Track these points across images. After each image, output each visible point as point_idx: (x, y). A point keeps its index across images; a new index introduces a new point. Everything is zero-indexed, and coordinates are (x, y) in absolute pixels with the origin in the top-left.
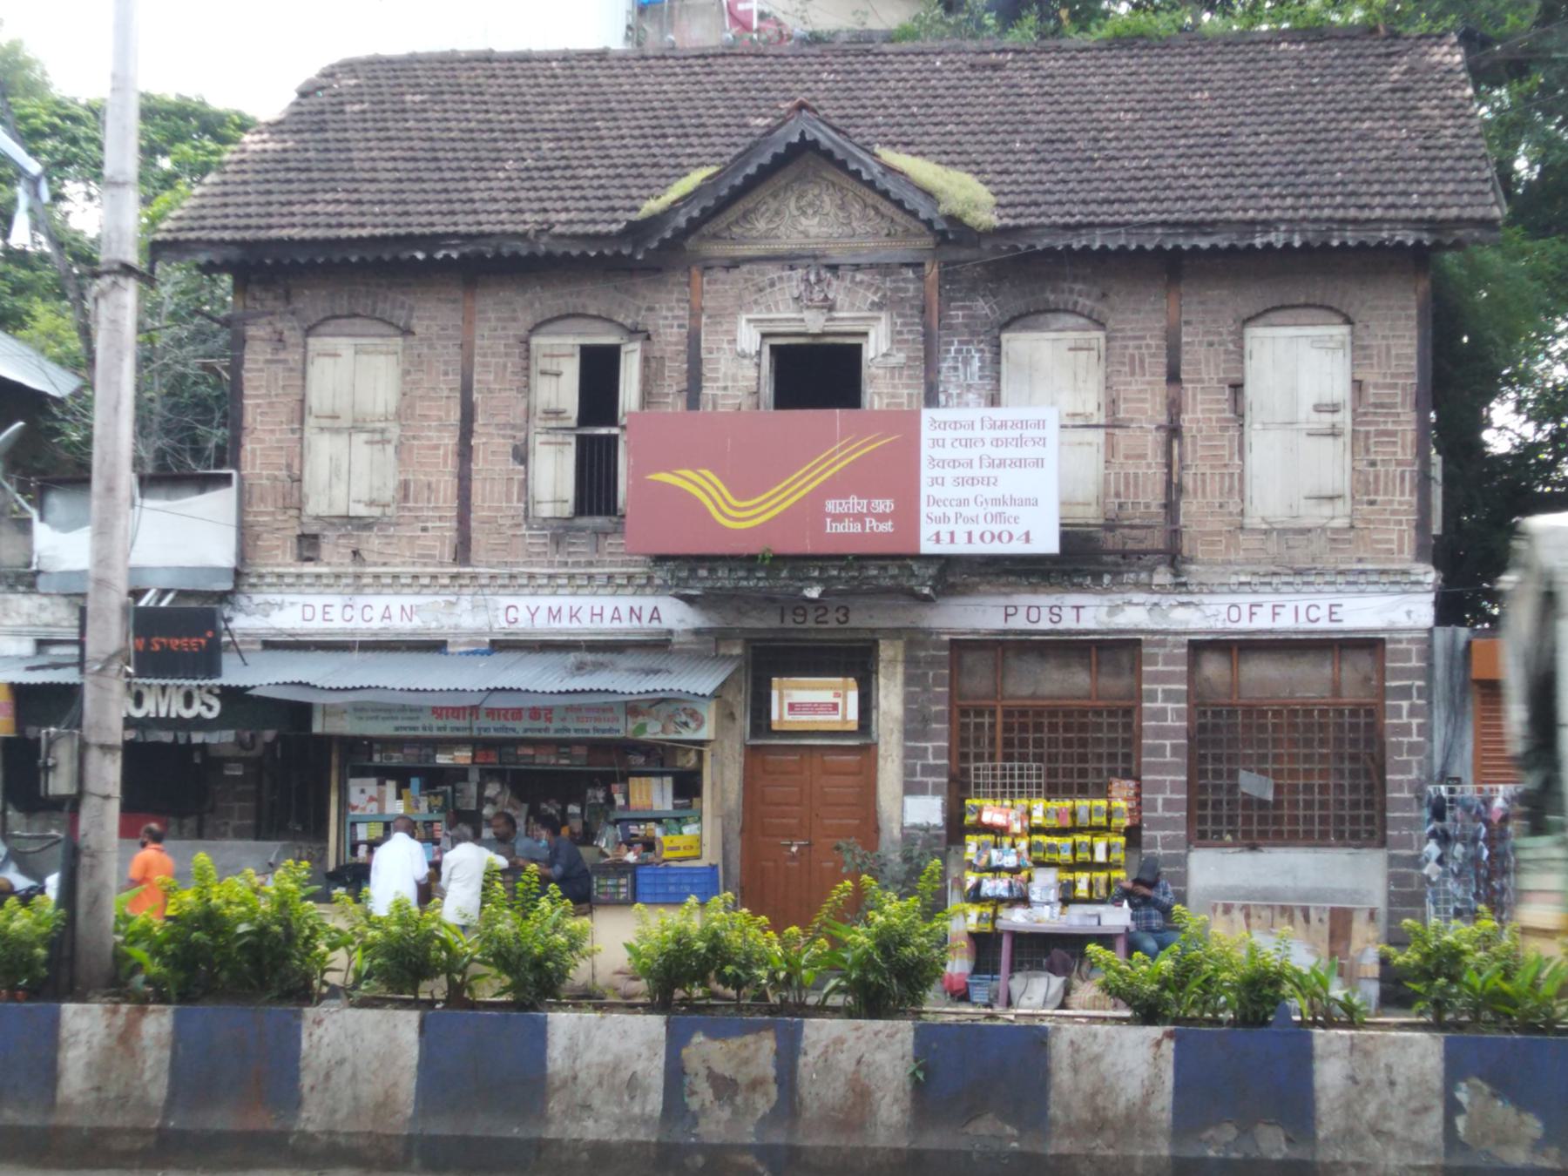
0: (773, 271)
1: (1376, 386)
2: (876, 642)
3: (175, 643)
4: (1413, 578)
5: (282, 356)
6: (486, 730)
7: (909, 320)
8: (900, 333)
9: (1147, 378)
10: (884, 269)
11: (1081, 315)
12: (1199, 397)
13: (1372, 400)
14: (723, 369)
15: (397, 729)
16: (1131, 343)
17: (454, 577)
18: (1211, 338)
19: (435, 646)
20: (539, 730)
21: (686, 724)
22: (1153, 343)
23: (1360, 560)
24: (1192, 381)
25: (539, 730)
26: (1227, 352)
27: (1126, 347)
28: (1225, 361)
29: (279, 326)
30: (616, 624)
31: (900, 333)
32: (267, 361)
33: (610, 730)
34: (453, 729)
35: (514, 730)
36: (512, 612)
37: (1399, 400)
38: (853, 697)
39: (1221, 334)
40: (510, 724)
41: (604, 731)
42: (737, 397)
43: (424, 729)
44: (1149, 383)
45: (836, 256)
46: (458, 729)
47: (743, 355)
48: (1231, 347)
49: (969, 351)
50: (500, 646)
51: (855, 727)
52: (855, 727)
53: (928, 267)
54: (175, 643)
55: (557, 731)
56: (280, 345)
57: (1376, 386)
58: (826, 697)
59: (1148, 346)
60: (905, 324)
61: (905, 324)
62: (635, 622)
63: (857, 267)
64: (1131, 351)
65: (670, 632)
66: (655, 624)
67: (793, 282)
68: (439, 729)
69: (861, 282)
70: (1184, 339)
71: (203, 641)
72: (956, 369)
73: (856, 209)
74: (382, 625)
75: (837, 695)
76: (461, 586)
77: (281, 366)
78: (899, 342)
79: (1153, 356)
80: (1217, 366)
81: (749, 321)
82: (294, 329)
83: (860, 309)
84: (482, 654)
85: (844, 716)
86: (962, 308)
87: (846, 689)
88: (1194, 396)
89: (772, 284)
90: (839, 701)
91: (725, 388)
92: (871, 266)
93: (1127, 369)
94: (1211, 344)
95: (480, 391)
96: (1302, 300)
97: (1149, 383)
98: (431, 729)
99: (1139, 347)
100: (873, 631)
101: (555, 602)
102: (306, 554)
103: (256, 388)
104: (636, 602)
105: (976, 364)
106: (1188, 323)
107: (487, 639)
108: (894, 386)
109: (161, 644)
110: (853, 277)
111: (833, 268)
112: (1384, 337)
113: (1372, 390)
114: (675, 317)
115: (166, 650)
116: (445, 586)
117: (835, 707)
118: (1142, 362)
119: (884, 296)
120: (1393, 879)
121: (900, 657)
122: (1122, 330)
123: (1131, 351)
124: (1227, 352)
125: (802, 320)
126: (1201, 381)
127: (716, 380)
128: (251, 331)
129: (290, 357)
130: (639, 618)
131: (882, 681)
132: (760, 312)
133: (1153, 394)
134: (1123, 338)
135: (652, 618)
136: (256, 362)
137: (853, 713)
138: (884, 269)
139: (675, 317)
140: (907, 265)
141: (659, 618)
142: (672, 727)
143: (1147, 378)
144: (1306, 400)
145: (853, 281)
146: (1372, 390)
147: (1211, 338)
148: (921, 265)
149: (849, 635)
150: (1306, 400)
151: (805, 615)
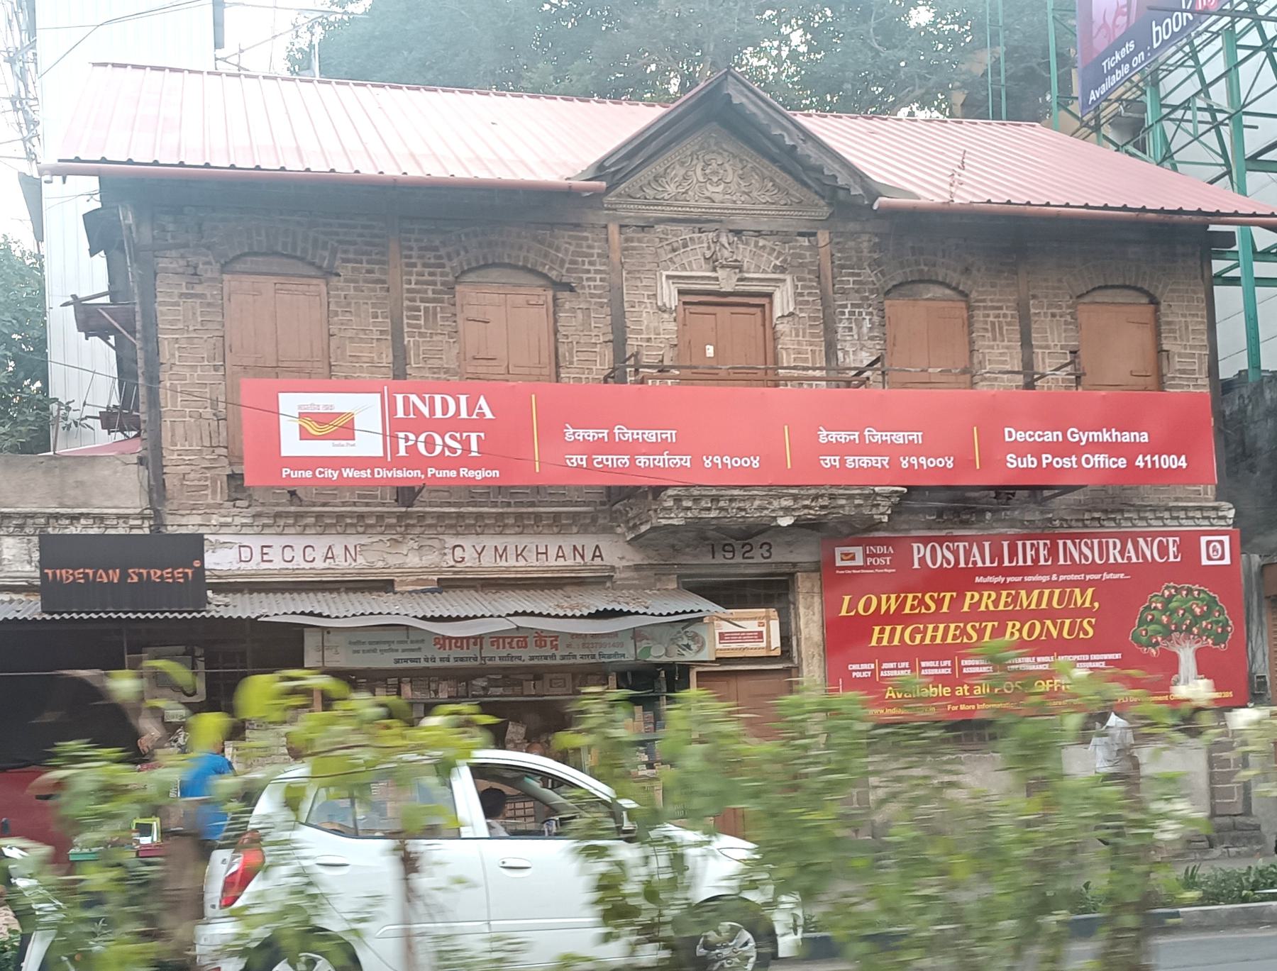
0: (685, 233)
1: (1180, 355)
2: (792, 575)
3: (156, 574)
4: (1221, 514)
5: (199, 289)
6: (491, 659)
7: (808, 283)
8: (801, 295)
9: (1006, 343)
10: (785, 237)
11: (948, 286)
12: (1047, 361)
13: (1178, 367)
14: (646, 322)
15: (397, 661)
16: (991, 312)
17: (400, 517)
18: (1054, 311)
19: (386, 586)
20: (546, 658)
21: (688, 646)
22: (1008, 312)
23: (1177, 500)
24: (1041, 347)
25: (546, 658)
26: (1066, 323)
27: (988, 316)
28: (1065, 331)
29: (192, 259)
30: (561, 562)
31: (801, 295)
32: (181, 295)
33: (616, 654)
34: (456, 659)
35: (519, 658)
36: (458, 551)
37: (1196, 367)
38: (775, 626)
39: (1060, 307)
40: (515, 652)
41: (609, 656)
42: (661, 348)
43: (426, 660)
44: (1007, 348)
45: (741, 222)
46: (462, 659)
47: (663, 309)
48: (1068, 318)
49: (860, 314)
50: (447, 585)
51: (778, 652)
52: (778, 652)
53: (819, 235)
54: (156, 574)
55: (563, 657)
56: (195, 279)
57: (1180, 355)
58: (752, 626)
59: (1005, 316)
60: (804, 287)
61: (804, 287)
62: (579, 559)
63: (759, 233)
64: (991, 319)
65: (613, 568)
66: (598, 561)
67: (702, 245)
68: (442, 659)
69: (764, 247)
70: (1033, 311)
71: (189, 571)
72: (850, 329)
73: (755, 180)
74: (326, 565)
75: (761, 625)
76: (407, 526)
77: (199, 301)
78: (801, 303)
79: (1009, 324)
80: (1059, 335)
81: (668, 277)
82: (209, 263)
83: (764, 271)
84: (432, 591)
85: (769, 643)
86: (853, 275)
87: (768, 618)
88: (1043, 359)
89: (685, 246)
90: (764, 629)
91: (649, 340)
92: (772, 233)
93: (989, 335)
94: (1053, 315)
95: (411, 335)
96: (1120, 282)
97: (1007, 348)
98: (433, 660)
99: (998, 316)
100: (794, 565)
101: (499, 541)
102: (234, 495)
103: (172, 322)
104: (579, 541)
105: (867, 324)
106: (1034, 297)
107: (435, 578)
108: (799, 343)
109: (140, 575)
110: (757, 243)
111: (738, 233)
112: (1184, 316)
113: (1177, 359)
114: (597, 272)
115: (145, 583)
116: (371, 526)
117: (760, 634)
118: (1001, 328)
119: (785, 261)
120: (1211, 762)
121: (816, 589)
122: (984, 301)
123: (991, 319)
124: (1066, 323)
125: (717, 279)
126: (1047, 347)
127: (640, 332)
128: (163, 263)
129: (207, 292)
130: (583, 557)
131: (802, 611)
132: (676, 270)
133: (1012, 358)
134: (985, 308)
135: (594, 556)
136: (170, 295)
137: (776, 642)
138: (785, 237)
139: (597, 272)
140: (801, 234)
141: (600, 556)
142: (675, 649)
143: (1006, 343)
144: (823, 440)
145: (756, 245)
146: (1177, 359)
147: (1054, 311)
148: (814, 234)
149: (773, 569)
150: (823, 440)
151: (733, 551)
